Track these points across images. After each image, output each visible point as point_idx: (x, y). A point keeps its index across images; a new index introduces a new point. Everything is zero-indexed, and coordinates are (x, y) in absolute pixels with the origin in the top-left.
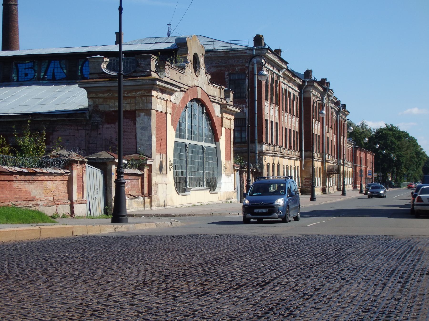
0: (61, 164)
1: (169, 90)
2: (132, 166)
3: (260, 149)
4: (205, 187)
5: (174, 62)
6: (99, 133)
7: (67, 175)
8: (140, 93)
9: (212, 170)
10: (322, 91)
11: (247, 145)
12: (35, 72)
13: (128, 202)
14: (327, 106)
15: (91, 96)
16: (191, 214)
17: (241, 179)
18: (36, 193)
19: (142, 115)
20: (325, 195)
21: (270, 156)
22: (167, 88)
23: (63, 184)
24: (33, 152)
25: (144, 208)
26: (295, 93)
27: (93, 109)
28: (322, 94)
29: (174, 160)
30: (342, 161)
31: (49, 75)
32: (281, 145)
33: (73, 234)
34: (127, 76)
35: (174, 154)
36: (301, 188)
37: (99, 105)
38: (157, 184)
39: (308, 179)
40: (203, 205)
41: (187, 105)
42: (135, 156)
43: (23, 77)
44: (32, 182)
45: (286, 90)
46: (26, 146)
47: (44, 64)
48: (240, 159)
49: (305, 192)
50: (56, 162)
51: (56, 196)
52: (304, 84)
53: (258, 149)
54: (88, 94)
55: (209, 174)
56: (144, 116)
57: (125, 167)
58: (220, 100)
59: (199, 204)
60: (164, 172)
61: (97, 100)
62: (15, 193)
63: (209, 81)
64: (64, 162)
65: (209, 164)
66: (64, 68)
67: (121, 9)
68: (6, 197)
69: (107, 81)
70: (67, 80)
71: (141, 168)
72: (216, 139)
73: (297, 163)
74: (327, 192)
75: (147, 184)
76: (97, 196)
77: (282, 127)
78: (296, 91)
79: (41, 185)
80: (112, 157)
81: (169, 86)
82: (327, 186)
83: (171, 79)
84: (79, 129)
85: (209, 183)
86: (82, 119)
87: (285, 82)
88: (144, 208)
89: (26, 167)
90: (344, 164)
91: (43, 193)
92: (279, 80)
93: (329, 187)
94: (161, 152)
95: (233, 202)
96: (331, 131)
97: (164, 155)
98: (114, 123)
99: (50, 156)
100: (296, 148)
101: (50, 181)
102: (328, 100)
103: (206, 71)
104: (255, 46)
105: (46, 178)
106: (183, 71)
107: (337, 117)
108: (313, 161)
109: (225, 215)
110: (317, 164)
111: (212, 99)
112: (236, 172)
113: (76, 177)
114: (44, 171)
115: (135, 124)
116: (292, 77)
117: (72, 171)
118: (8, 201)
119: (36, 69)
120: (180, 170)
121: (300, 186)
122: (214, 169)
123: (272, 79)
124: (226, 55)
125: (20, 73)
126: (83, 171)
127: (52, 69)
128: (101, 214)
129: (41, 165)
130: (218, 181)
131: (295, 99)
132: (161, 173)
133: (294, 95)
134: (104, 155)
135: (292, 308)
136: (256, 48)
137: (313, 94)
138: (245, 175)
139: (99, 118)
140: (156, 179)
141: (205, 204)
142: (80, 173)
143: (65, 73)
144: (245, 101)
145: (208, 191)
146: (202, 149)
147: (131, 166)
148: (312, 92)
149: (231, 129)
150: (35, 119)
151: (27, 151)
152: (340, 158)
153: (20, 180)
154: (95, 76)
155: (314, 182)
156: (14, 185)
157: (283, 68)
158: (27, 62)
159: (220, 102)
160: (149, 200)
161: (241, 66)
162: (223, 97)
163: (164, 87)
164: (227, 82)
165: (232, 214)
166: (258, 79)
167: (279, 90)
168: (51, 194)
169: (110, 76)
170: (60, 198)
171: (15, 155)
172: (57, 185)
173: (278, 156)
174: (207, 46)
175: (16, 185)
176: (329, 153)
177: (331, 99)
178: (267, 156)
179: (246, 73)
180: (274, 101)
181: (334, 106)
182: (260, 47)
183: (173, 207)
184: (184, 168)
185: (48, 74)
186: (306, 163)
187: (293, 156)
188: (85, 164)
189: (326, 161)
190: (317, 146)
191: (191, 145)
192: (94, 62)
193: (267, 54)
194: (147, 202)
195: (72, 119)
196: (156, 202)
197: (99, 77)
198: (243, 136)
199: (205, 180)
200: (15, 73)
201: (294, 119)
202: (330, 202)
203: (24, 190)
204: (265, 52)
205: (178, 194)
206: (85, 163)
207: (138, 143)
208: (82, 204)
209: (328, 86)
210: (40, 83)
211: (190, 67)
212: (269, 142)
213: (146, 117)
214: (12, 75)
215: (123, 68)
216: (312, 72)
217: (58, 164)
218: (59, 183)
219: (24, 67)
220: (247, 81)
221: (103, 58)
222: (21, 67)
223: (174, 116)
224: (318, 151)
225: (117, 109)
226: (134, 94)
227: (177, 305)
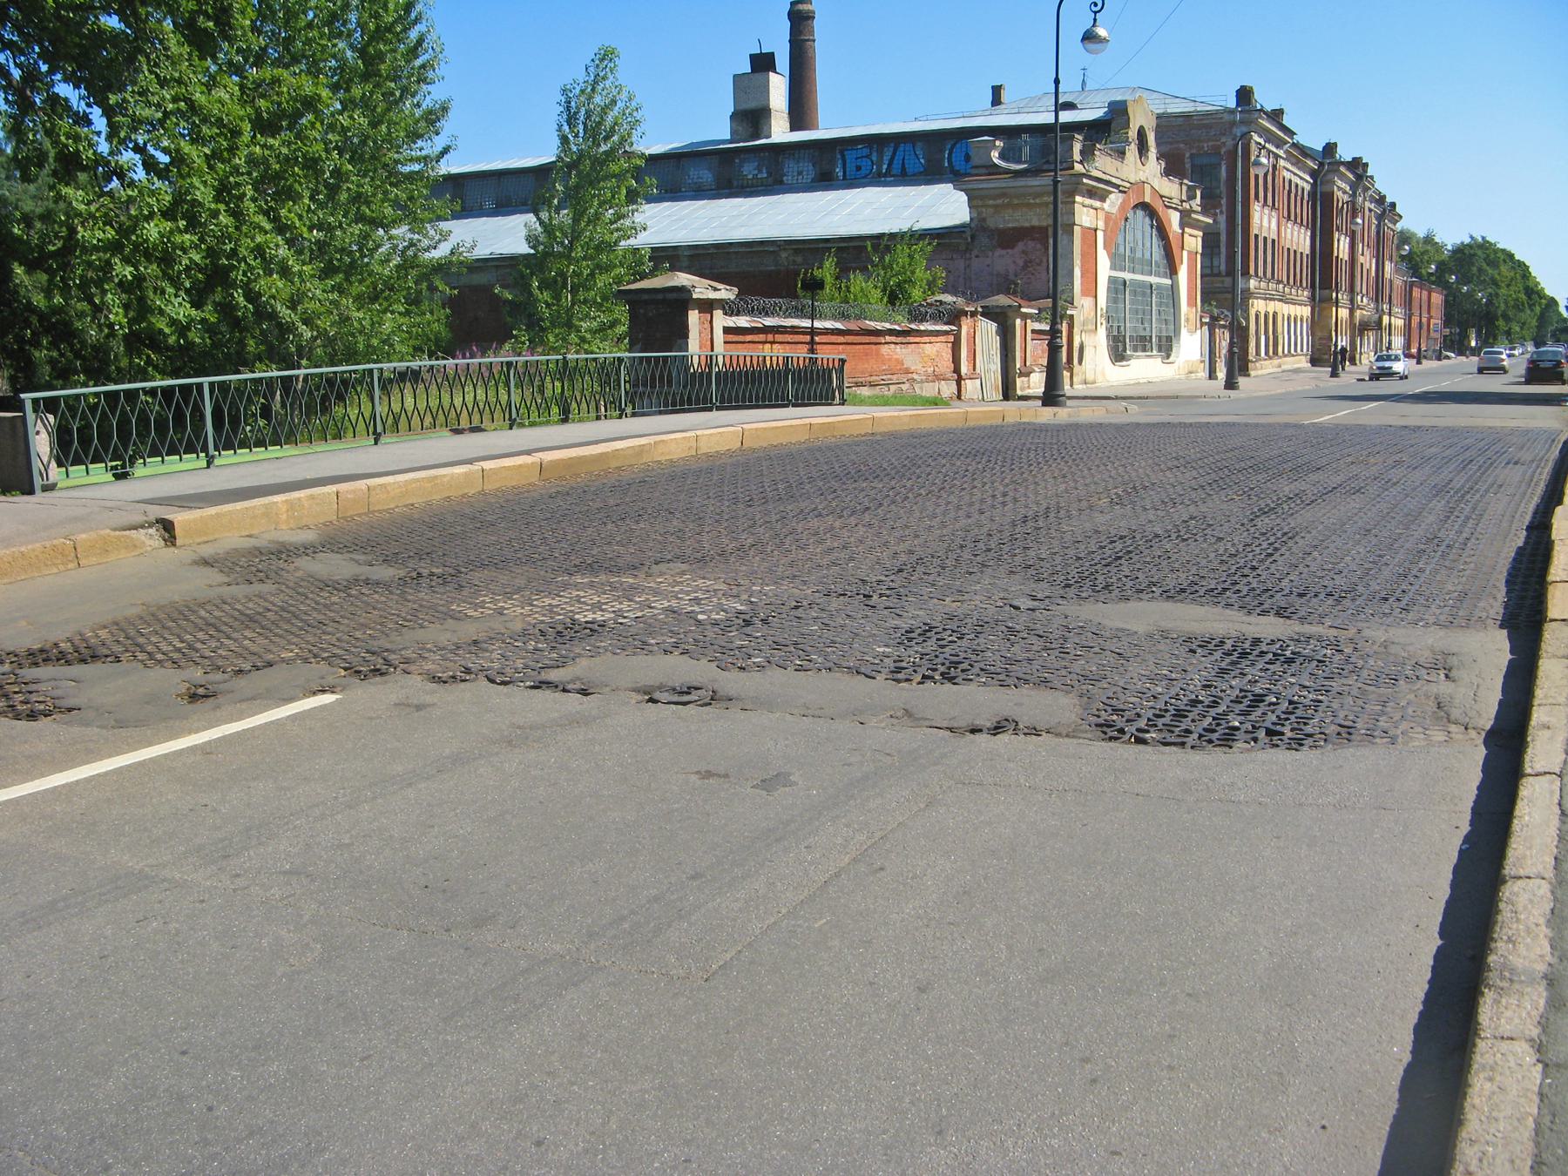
3: (1244, 286)
4: (1155, 352)
15: (975, 203)
28: (1354, 187)
29: (1107, 307)
31: (896, 168)
45: (1290, 181)
55: (1161, 331)
59: (1145, 381)
72: (1173, 271)
73: (1306, 311)
74: (1358, 362)
78: (1307, 182)
87: (1289, 166)
96: (1367, 252)
100: (1304, 285)
104: (1238, 105)
105: (926, 339)
107: (1378, 226)
114: (922, 328)
117: (960, 327)
119: (874, 158)
120: (1115, 325)
133: (1303, 189)
158: (860, 147)
162: (1184, 198)
163: (1094, 187)
173: (1274, 299)
176: (1364, 291)
178: (1257, 298)
182: (1247, 108)
189: (1358, 306)
201: (1303, 231)
211: (1132, 151)
212: (1261, 273)
223: (1109, 233)
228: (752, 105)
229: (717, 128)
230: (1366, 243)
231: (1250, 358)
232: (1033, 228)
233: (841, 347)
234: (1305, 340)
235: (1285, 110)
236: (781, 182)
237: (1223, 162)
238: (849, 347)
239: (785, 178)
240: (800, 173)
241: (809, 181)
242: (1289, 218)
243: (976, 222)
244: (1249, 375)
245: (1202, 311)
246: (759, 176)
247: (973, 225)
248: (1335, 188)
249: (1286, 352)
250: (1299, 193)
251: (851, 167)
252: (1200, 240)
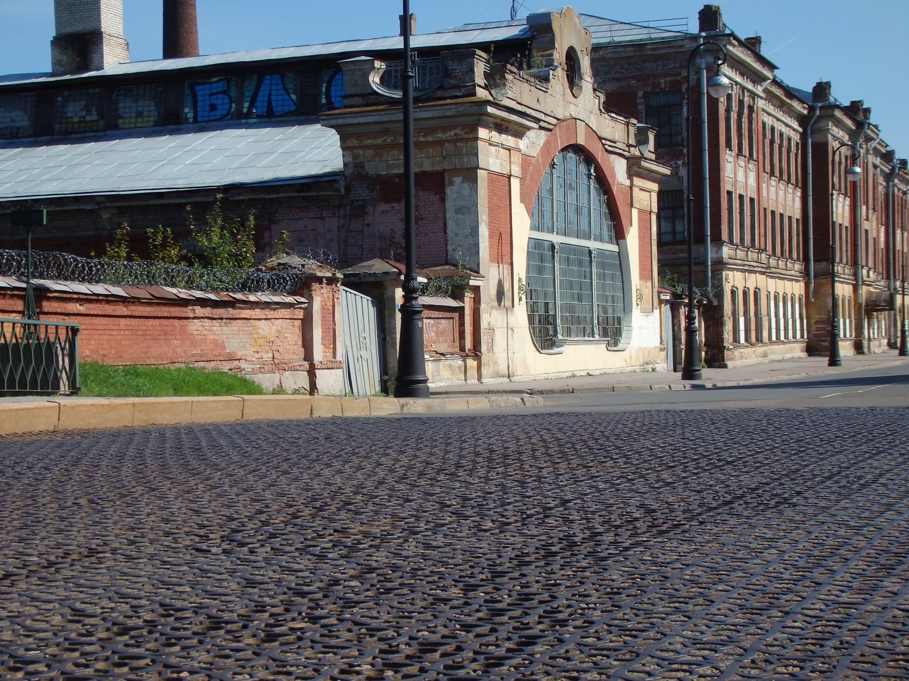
0: (287, 284)
1: (515, 127)
2: (439, 291)
3: (715, 256)
4: (597, 337)
5: (525, 67)
6: (366, 222)
7: (301, 308)
8: (453, 133)
9: (610, 299)
10: (854, 128)
11: (685, 247)
12: (231, 102)
13: (430, 367)
14: (864, 162)
15: (349, 143)
16: (566, 388)
17: (676, 321)
18: (236, 345)
19: (458, 180)
20: (861, 357)
21: (737, 270)
22: (509, 121)
23: (292, 327)
24: (229, 262)
25: (465, 380)
26: (792, 134)
27: (353, 172)
28: (853, 135)
29: (528, 278)
30: (898, 284)
31: (261, 107)
32: (763, 247)
33: (311, 413)
34: (424, 97)
35: (528, 265)
36: (808, 343)
37: (366, 164)
38: (492, 330)
39: (822, 322)
40: (592, 375)
41: (555, 160)
42: (445, 269)
43: (206, 114)
44: (228, 321)
45: (773, 128)
46: (214, 249)
47: (250, 84)
48: (672, 279)
49: (817, 350)
50: (278, 280)
51: (278, 351)
52: (812, 113)
53: (710, 255)
54: (341, 139)
55: (605, 311)
56: (463, 182)
57: (424, 293)
58: (627, 149)
59: (584, 373)
60: (508, 303)
61: (361, 152)
62: (193, 344)
63: (601, 107)
64: (294, 280)
65: (603, 287)
66: (291, 91)
68: (175, 351)
69: (382, 110)
70: (297, 115)
71: (457, 294)
72: (619, 234)
73: (798, 288)
74: (866, 350)
75: (472, 328)
76: (364, 354)
77: (765, 209)
78: (794, 130)
79: (248, 329)
80: (395, 270)
81: (514, 118)
82: (866, 337)
83: (518, 103)
84: (324, 215)
85: (605, 330)
86: (331, 193)
87: (771, 109)
88: (465, 380)
89: (214, 290)
90: (903, 291)
91: (251, 345)
92: (755, 106)
93: (869, 339)
94: (500, 260)
95: (658, 369)
96: (873, 217)
97: (506, 266)
98: (399, 202)
99: (264, 269)
100: (795, 256)
101: (265, 319)
102: (867, 148)
103: (596, 86)
104: (701, 30)
105: (257, 313)
106: (544, 85)
107: (887, 187)
108: (833, 282)
109: (640, 389)
110: (843, 290)
111: (610, 146)
112: (663, 305)
113: (320, 312)
114: (252, 298)
115: (443, 200)
116: (784, 98)
117: (310, 298)
118: (179, 360)
119: (233, 95)
120: (541, 301)
121: (805, 337)
122: (615, 300)
123: (741, 103)
124: (639, 53)
125: (199, 104)
126: (333, 300)
127: (267, 93)
128: (373, 393)
129: (244, 287)
130: (624, 324)
131: (793, 148)
132: (500, 305)
133: (789, 139)
134: (378, 266)
135: (786, 495)
136: (704, 34)
137: (832, 135)
138: (683, 310)
139: (366, 191)
140: (489, 319)
141: (597, 373)
142: (328, 304)
143: (293, 100)
144: (682, 151)
145: (603, 346)
146: (588, 255)
147: (437, 290)
148: (831, 132)
149: (651, 212)
150: (232, 197)
151: (216, 260)
152: (894, 277)
153: (202, 318)
154: (356, 100)
155: (836, 324)
156: (190, 328)
157: (765, 79)
158: (214, 79)
159: (626, 154)
160: (475, 363)
161: (672, 75)
162: (632, 141)
163: (503, 119)
164: (642, 113)
165: (656, 386)
166: (708, 93)
167: (757, 127)
168: (267, 348)
169: (388, 100)
170: (287, 357)
171: (191, 264)
172: (280, 329)
173: (755, 272)
174: (598, 35)
175: (194, 328)
176: (871, 264)
177: (873, 146)
178: (733, 270)
179: (683, 91)
180: (746, 151)
181: (880, 163)
182: (713, 33)
183: (528, 379)
184: (550, 295)
185: (258, 104)
186: (818, 286)
187: (789, 272)
188: (339, 285)
189: (863, 281)
190: (841, 250)
191: (565, 246)
192: (354, 70)
193: (730, 48)
194: (472, 367)
195: (310, 194)
196: (491, 368)
197: (364, 102)
198: (679, 228)
199: (595, 322)
200: (189, 104)
201: (790, 191)
202: (873, 367)
203: (211, 337)
204: (724, 42)
205: (538, 350)
206: (338, 282)
207: (449, 242)
208: (333, 368)
209: (867, 117)
210: (242, 124)
211: (559, 78)
212: (736, 239)
213: (466, 185)
214: (183, 110)
215: (413, 83)
216: (830, 87)
217: (281, 284)
218: (284, 325)
219: (208, 92)
220: (685, 109)
221: (372, 62)
222: (202, 91)
223: (527, 182)
224: (844, 261)
225: (401, 170)
226: (441, 136)
227: (528, 494)
228: (78, 27)
230: (871, 206)
231: (726, 344)
233: (123, 321)
234: (798, 327)
235: (763, 40)
237: (685, 102)
238: (134, 322)
239: (120, 121)
240: (139, 114)
241: (151, 124)
242: (772, 174)
244: (725, 366)
245: (659, 287)
246: (88, 118)
247: (347, 173)
248: (830, 137)
249: (774, 338)
250: (785, 143)
252: (654, 196)
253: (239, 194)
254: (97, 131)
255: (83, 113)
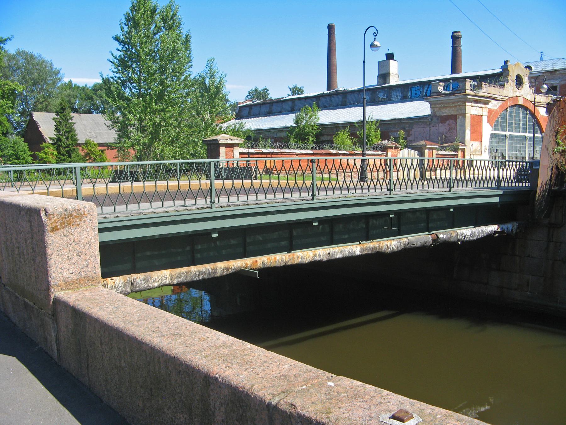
61: (435, 109)
67: (364, 62)
119: (421, 90)
219: (415, 90)
226: (456, 104)
229: (372, 81)
232: (452, 115)
236: (391, 100)
239: (392, 98)
240: (397, 96)
243: (432, 114)
251: (413, 94)
253: (404, 121)
254: (386, 101)
255: (383, 96)
